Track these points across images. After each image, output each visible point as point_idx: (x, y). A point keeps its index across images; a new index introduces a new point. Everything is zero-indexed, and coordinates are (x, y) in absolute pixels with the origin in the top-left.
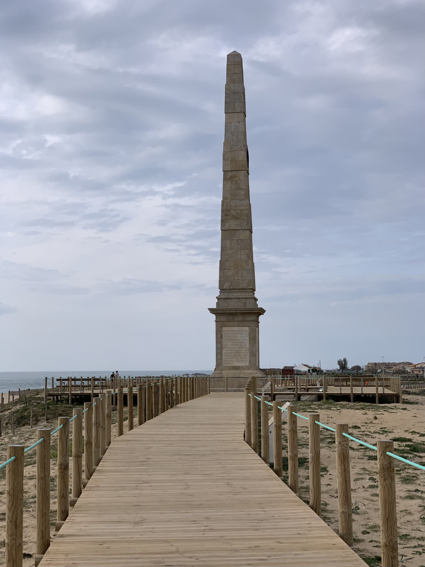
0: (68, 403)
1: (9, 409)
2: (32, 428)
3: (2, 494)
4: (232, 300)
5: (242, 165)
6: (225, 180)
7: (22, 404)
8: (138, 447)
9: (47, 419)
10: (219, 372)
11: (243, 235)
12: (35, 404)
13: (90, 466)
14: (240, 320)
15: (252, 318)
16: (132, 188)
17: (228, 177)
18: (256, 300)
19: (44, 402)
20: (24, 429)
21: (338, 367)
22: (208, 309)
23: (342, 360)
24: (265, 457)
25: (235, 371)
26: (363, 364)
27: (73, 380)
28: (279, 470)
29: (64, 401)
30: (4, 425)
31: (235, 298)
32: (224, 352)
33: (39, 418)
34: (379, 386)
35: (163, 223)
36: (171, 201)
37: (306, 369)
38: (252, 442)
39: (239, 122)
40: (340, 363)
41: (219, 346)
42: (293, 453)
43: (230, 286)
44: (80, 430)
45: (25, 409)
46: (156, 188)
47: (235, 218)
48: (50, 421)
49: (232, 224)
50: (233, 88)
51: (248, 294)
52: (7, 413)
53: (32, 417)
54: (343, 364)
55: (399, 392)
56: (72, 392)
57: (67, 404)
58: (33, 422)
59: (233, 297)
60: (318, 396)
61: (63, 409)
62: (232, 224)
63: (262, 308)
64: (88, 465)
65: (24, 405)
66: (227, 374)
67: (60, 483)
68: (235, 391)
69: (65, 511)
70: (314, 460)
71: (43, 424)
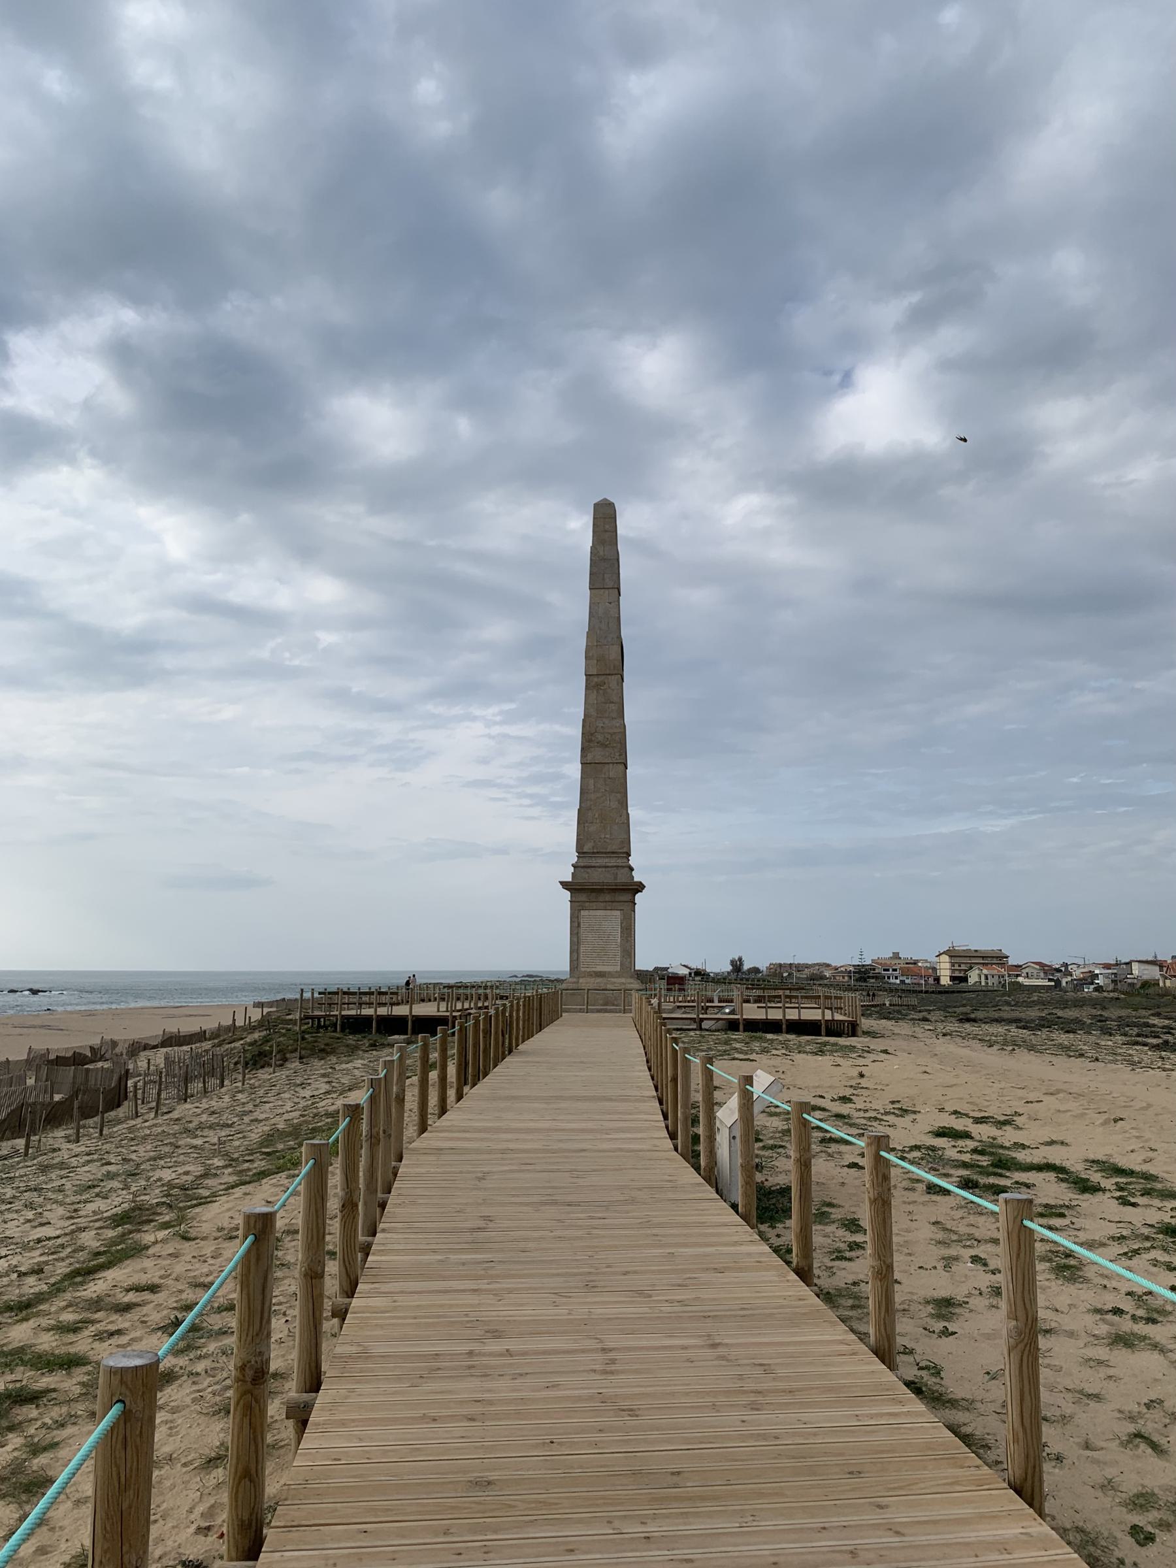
0: (335, 1031)
1: (242, 1039)
2: (274, 1072)
3: (155, 1293)
4: (597, 869)
5: (614, 667)
6: (587, 688)
7: (262, 1031)
8: (461, 1172)
9: (301, 1058)
10: (575, 980)
11: (613, 771)
12: (284, 1031)
13: (352, 1262)
14: (607, 900)
15: (626, 897)
16: (440, 710)
17: (593, 684)
18: (632, 869)
19: (297, 1028)
20: (264, 1074)
21: (729, 968)
22: (560, 882)
23: (737, 959)
24: (748, 1213)
25: (599, 980)
26: (763, 965)
27: (345, 993)
28: (806, 1269)
29: (329, 1026)
30: (232, 1066)
31: (600, 867)
32: (582, 949)
33: (288, 1056)
34: (826, 1008)
35: (485, 761)
36: (496, 730)
37: (686, 971)
38: (703, 1163)
39: (610, 603)
40: (733, 963)
41: (576, 940)
42: (884, 1262)
43: (593, 847)
44: (319, 1200)
45: (266, 1040)
46: (477, 711)
47: (603, 745)
48: (304, 1060)
49: (597, 755)
50: (601, 553)
51: (619, 861)
52: (238, 1044)
53: (275, 1056)
54: (737, 965)
55: (856, 1018)
56: (344, 1013)
57: (334, 1032)
58: (278, 1063)
59: (598, 864)
60: (730, 1022)
61: (327, 1041)
62: (597, 755)
63: (641, 883)
64: (346, 1259)
65: (265, 1032)
66: (587, 983)
67: (236, 1427)
68: (599, 1011)
69: (250, 1524)
70: (1023, 1339)
71: (293, 1066)
